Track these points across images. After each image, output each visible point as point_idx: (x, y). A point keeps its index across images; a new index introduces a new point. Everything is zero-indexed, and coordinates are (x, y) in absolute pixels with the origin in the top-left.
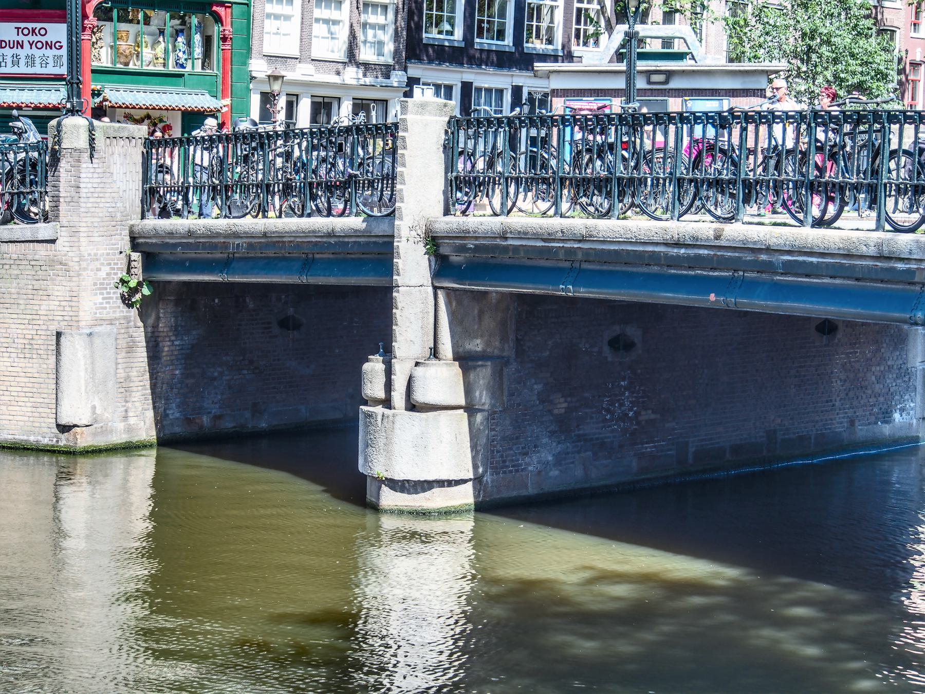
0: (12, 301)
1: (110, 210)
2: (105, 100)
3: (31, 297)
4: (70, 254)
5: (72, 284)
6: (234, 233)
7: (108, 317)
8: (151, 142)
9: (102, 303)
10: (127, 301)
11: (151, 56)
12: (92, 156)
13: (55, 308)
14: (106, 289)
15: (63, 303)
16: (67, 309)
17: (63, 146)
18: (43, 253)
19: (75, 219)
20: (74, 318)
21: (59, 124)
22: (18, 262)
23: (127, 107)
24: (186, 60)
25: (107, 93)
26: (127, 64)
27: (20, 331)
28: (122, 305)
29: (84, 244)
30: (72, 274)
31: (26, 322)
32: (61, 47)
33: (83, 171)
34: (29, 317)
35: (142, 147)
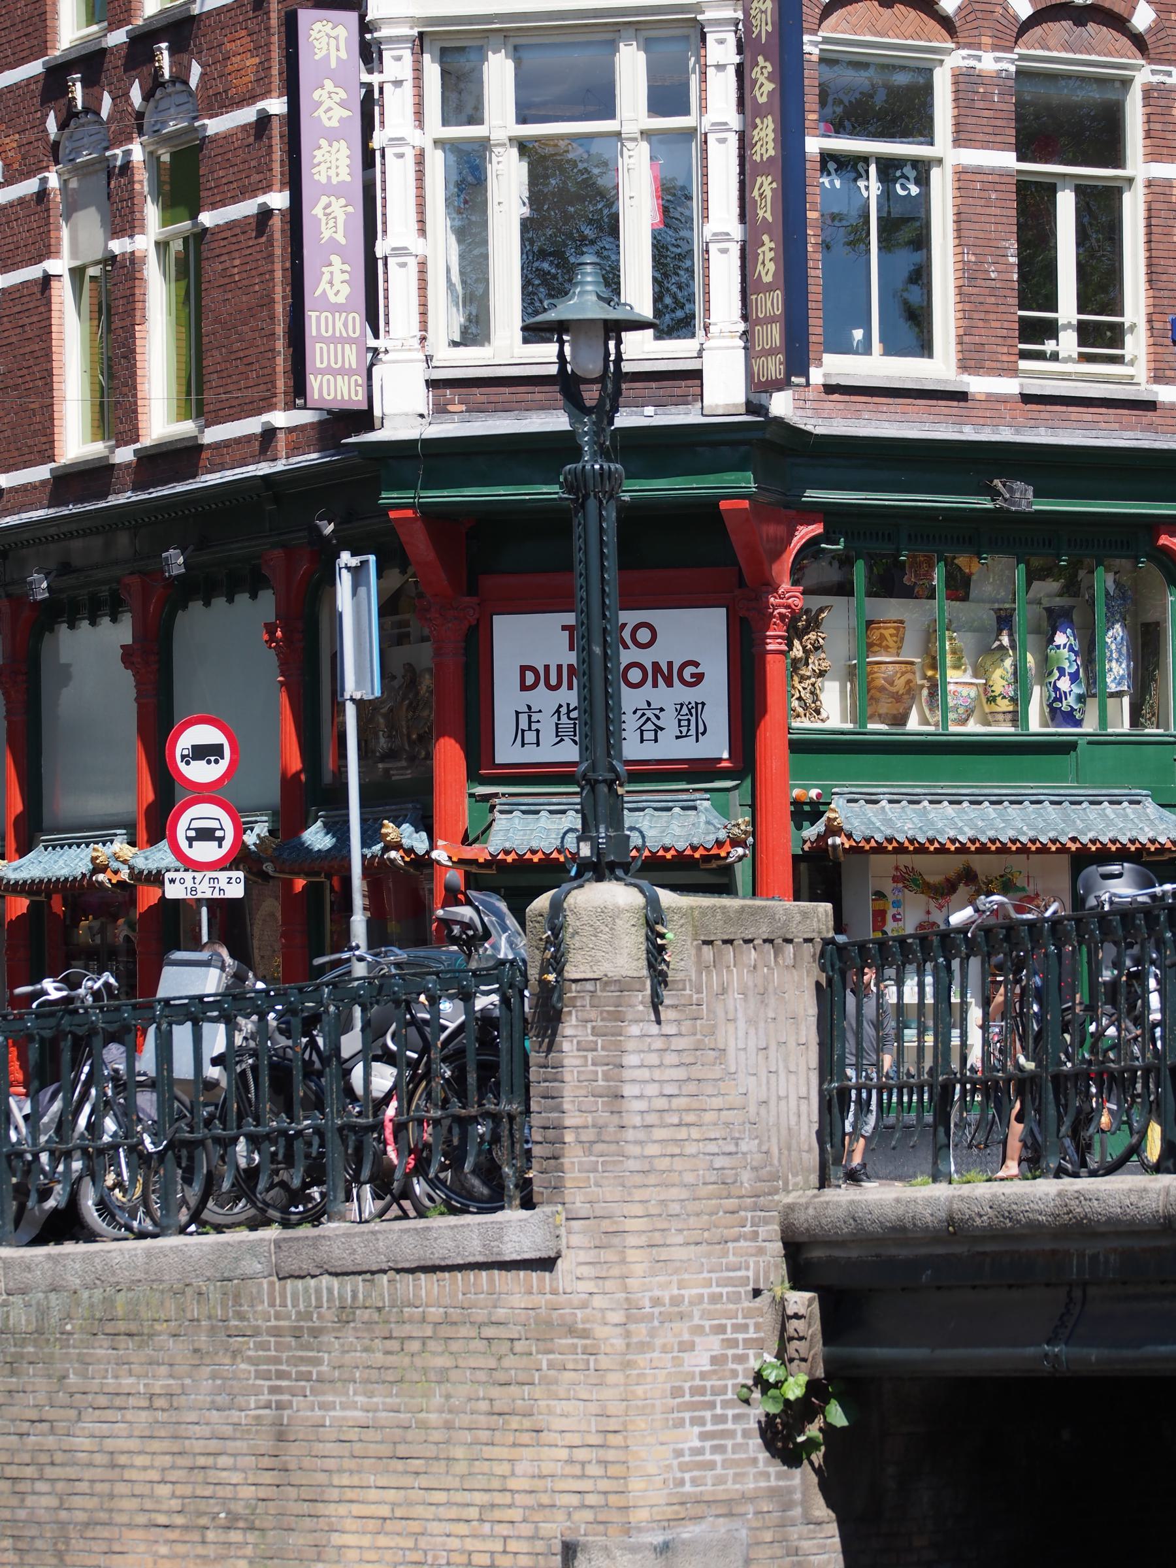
0: (431, 1451)
1: (719, 1162)
2: (833, 830)
3: (484, 1435)
4: (598, 1301)
5: (607, 1393)
6: (1079, 1223)
7: (721, 1492)
8: (841, 949)
9: (699, 1451)
10: (781, 1439)
11: (969, 696)
12: (656, 1003)
13: (558, 1469)
14: (711, 1405)
15: (581, 1454)
16: (593, 1470)
17: (571, 972)
18: (519, 1301)
19: (610, 1192)
20: (612, 1499)
21: (557, 907)
22: (446, 1331)
23: (900, 849)
24: (1081, 699)
25: (840, 810)
26: (901, 720)
27: (454, 1543)
28: (764, 1455)
29: (639, 1269)
30: (604, 1362)
31: (473, 1513)
32: (699, 678)
33: (630, 1045)
34: (479, 1498)
35: (815, 968)
